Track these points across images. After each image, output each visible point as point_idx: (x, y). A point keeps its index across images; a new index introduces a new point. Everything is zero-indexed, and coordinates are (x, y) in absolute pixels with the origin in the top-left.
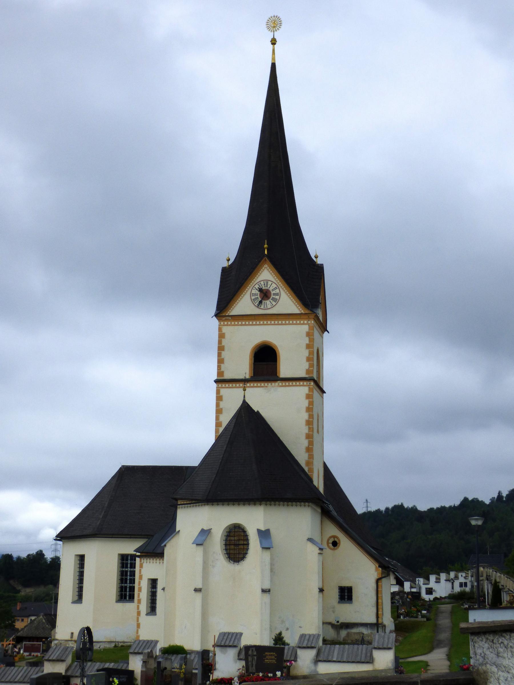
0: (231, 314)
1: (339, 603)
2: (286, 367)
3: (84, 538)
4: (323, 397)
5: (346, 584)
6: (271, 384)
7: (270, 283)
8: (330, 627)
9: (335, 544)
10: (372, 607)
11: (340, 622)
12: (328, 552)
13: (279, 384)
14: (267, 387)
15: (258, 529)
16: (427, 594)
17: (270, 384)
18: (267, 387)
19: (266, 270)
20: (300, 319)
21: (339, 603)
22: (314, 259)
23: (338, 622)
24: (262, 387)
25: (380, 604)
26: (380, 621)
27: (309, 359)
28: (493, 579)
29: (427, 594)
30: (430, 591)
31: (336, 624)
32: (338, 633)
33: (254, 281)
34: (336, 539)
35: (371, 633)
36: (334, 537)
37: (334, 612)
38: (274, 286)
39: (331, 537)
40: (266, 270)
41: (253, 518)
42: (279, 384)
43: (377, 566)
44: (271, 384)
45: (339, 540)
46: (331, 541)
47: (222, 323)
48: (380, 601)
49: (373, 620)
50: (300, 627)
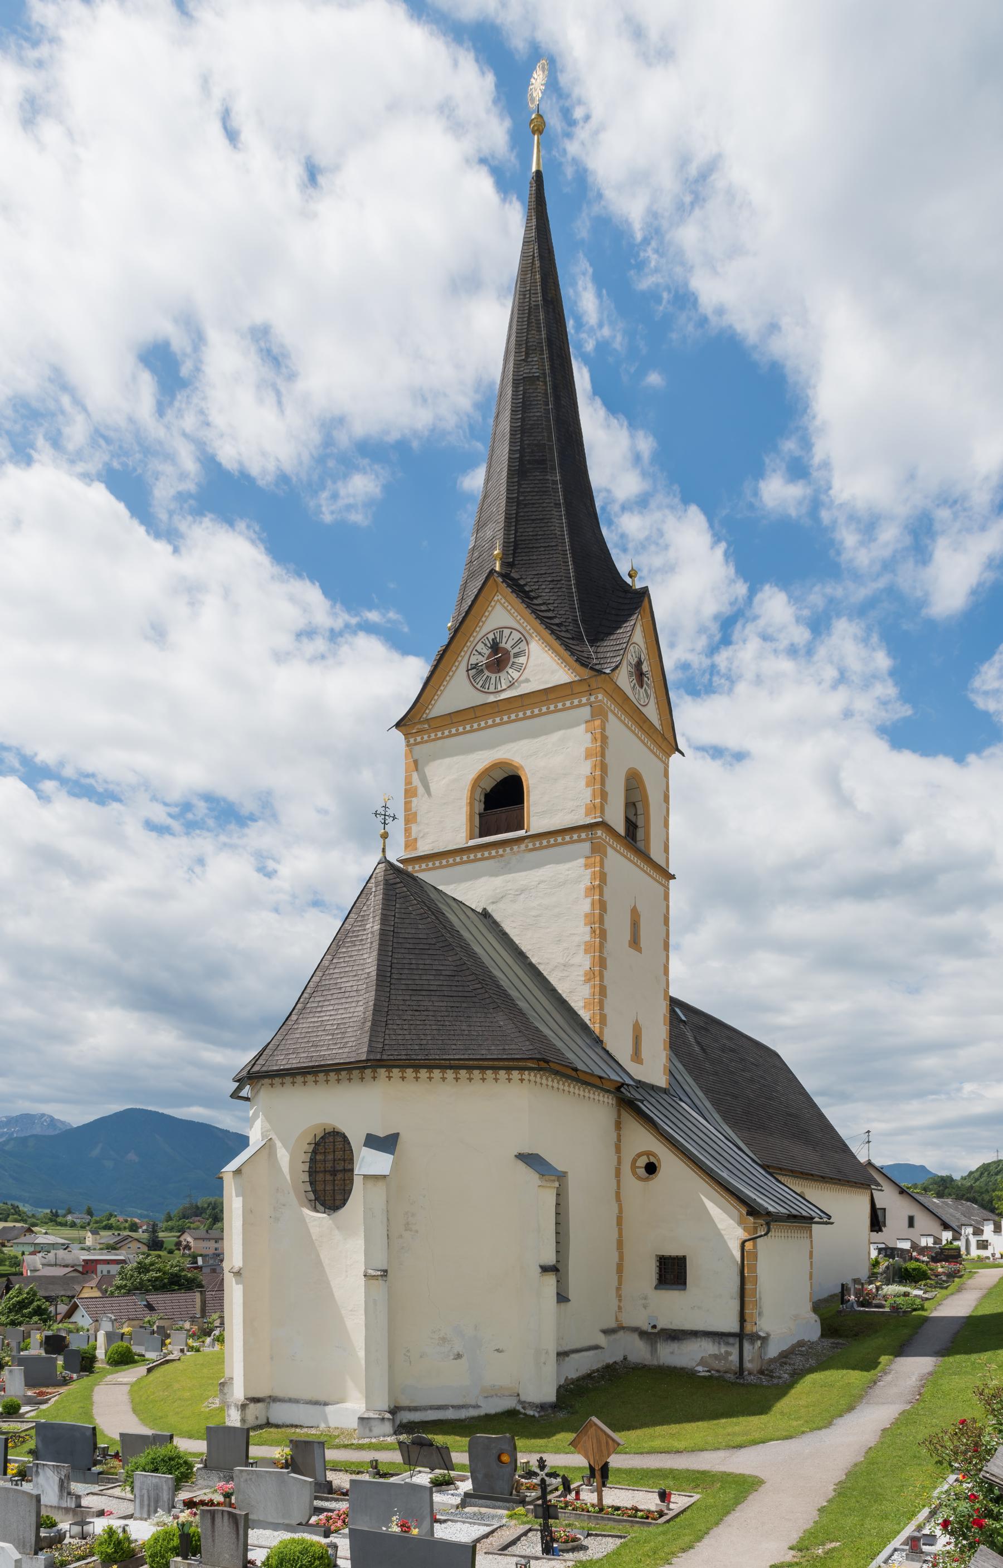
0: (431, 716)
1: (656, 1288)
2: (546, 807)
3: (851, 1186)
4: (667, 888)
5: (672, 1250)
6: (512, 849)
7: (506, 632)
8: (636, 1336)
9: (651, 1169)
10: (732, 1298)
11: (659, 1327)
12: (632, 1185)
13: (527, 846)
14: (502, 856)
15: (398, 1134)
16: (978, 1248)
17: (508, 849)
18: (502, 856)
19: (498, 607)
20: (573, 695)
21: (656, 1288)
22: (629, 581)
23: (654, 1327)
24: (494, 857)
25: (747, 1292)
26: (749, 1328)
27: (591, 781)
28: (458, 1483)
29: (978, 1248)
30: (983, 1245)
31: (650, 1330)
32: (654, 1351)
33: (475, 637)
34: (653, 1159)
35: (727, 1352)
36: (648, 1154)
37: (645, 1307)
38: (516, 636)
39: (640, 1155)
40: (498, 607)
41: (354, 1109)
42: (527, 846)
43: (744, 1213)
44: (512, 849)
45: (659, 1160)
46: (643, 1161)
47: (412, 741)
48: (748, 1286)
49: (734, 1327)
50: (459, 1356)
